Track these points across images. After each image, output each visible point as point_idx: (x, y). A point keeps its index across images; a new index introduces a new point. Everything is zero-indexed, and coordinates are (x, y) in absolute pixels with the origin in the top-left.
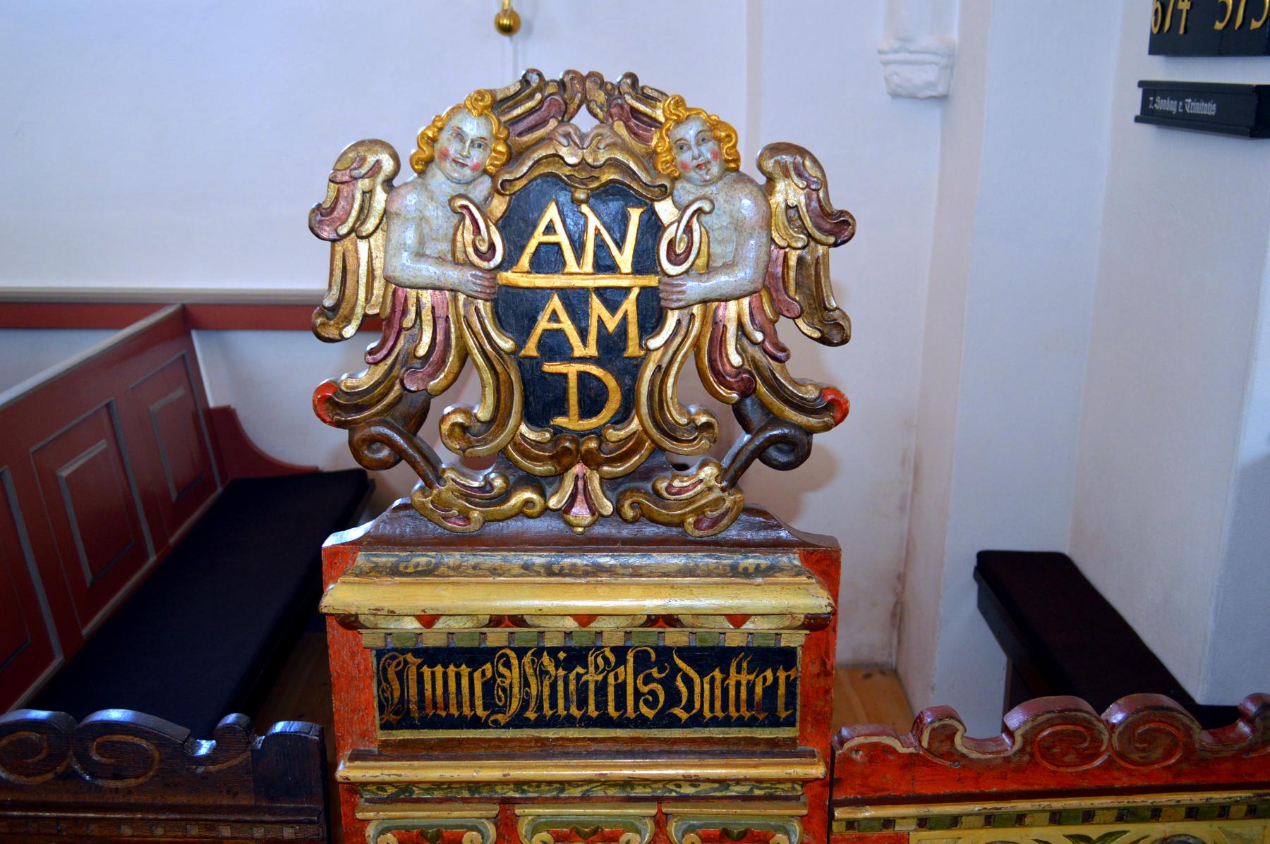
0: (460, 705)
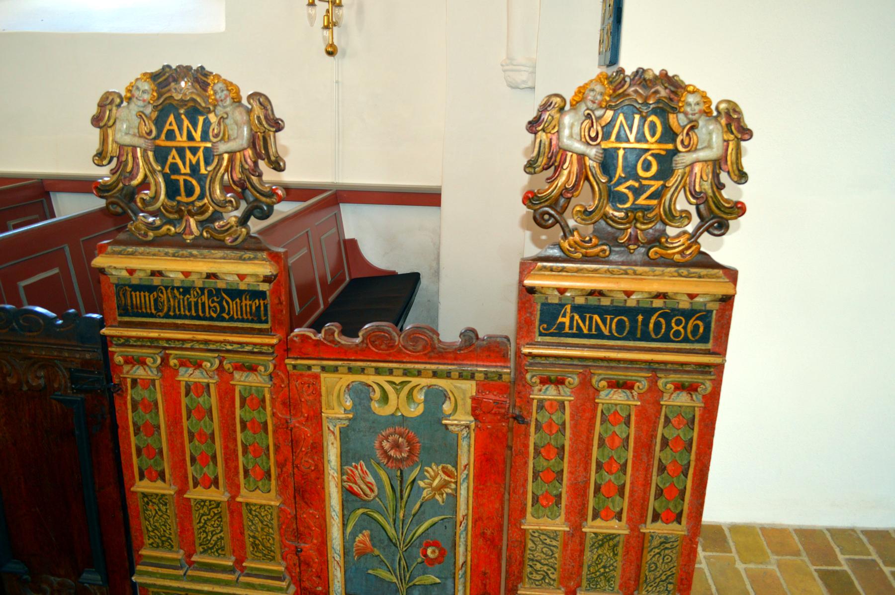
0: (146, 308)
